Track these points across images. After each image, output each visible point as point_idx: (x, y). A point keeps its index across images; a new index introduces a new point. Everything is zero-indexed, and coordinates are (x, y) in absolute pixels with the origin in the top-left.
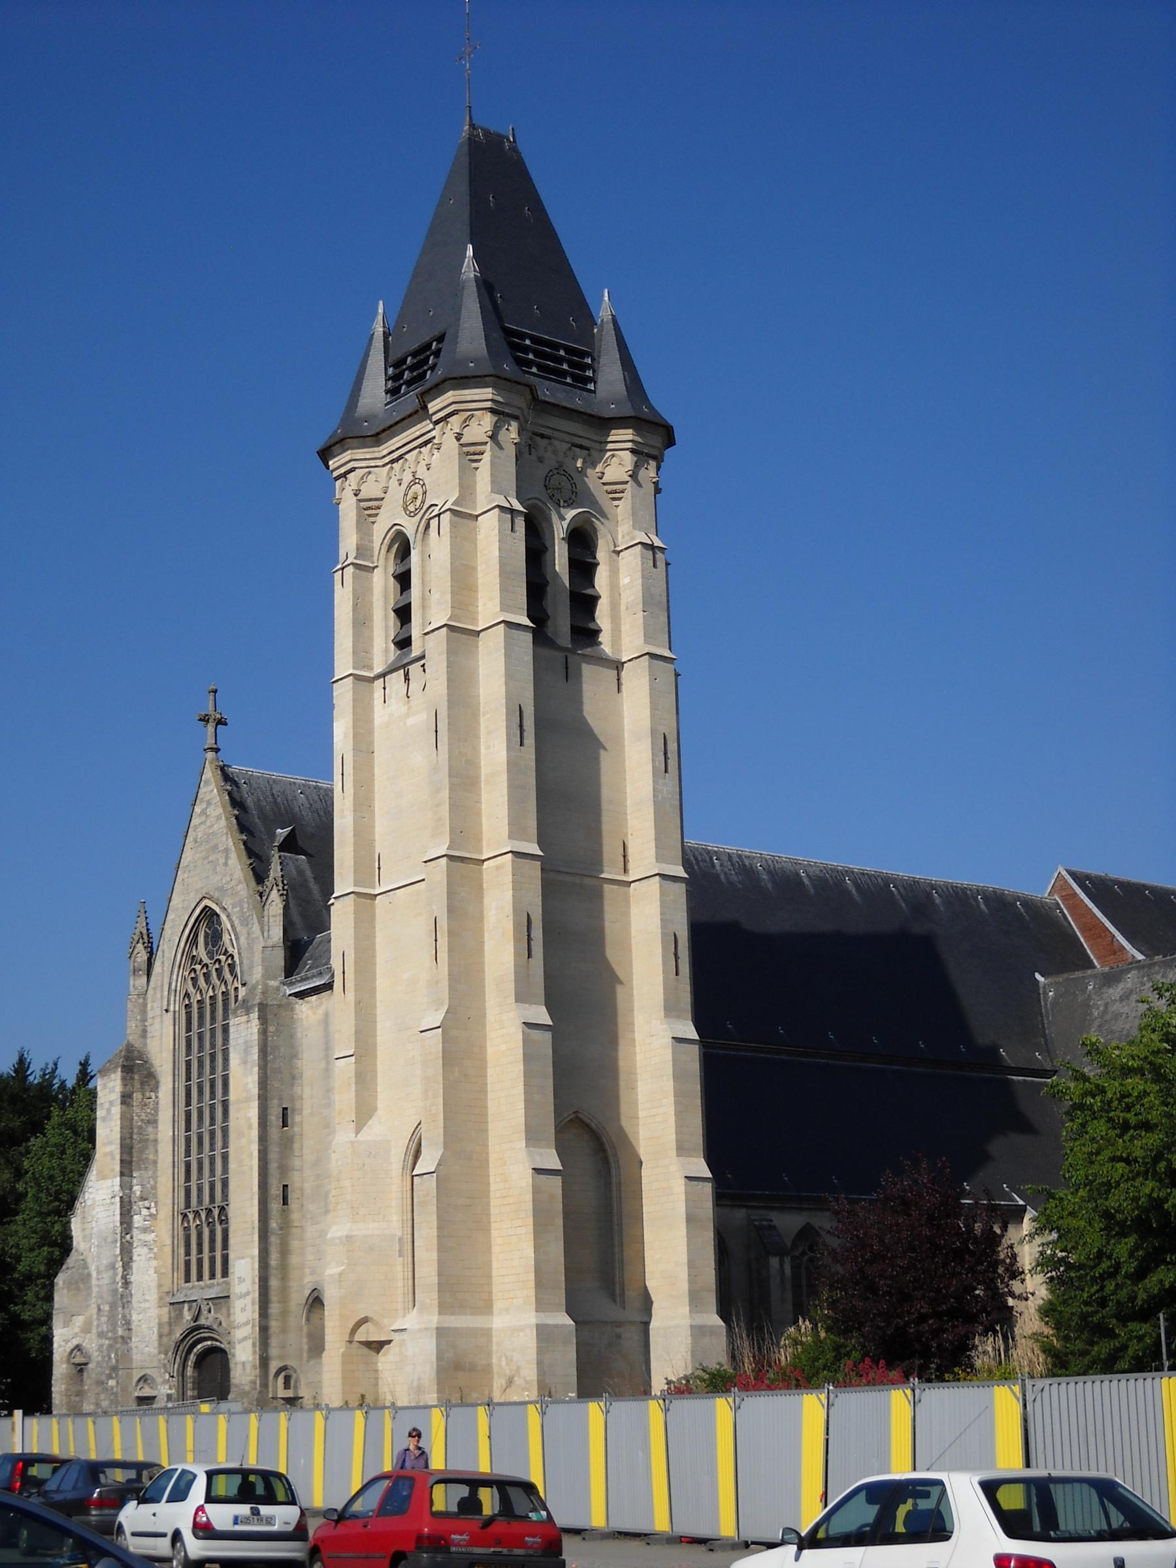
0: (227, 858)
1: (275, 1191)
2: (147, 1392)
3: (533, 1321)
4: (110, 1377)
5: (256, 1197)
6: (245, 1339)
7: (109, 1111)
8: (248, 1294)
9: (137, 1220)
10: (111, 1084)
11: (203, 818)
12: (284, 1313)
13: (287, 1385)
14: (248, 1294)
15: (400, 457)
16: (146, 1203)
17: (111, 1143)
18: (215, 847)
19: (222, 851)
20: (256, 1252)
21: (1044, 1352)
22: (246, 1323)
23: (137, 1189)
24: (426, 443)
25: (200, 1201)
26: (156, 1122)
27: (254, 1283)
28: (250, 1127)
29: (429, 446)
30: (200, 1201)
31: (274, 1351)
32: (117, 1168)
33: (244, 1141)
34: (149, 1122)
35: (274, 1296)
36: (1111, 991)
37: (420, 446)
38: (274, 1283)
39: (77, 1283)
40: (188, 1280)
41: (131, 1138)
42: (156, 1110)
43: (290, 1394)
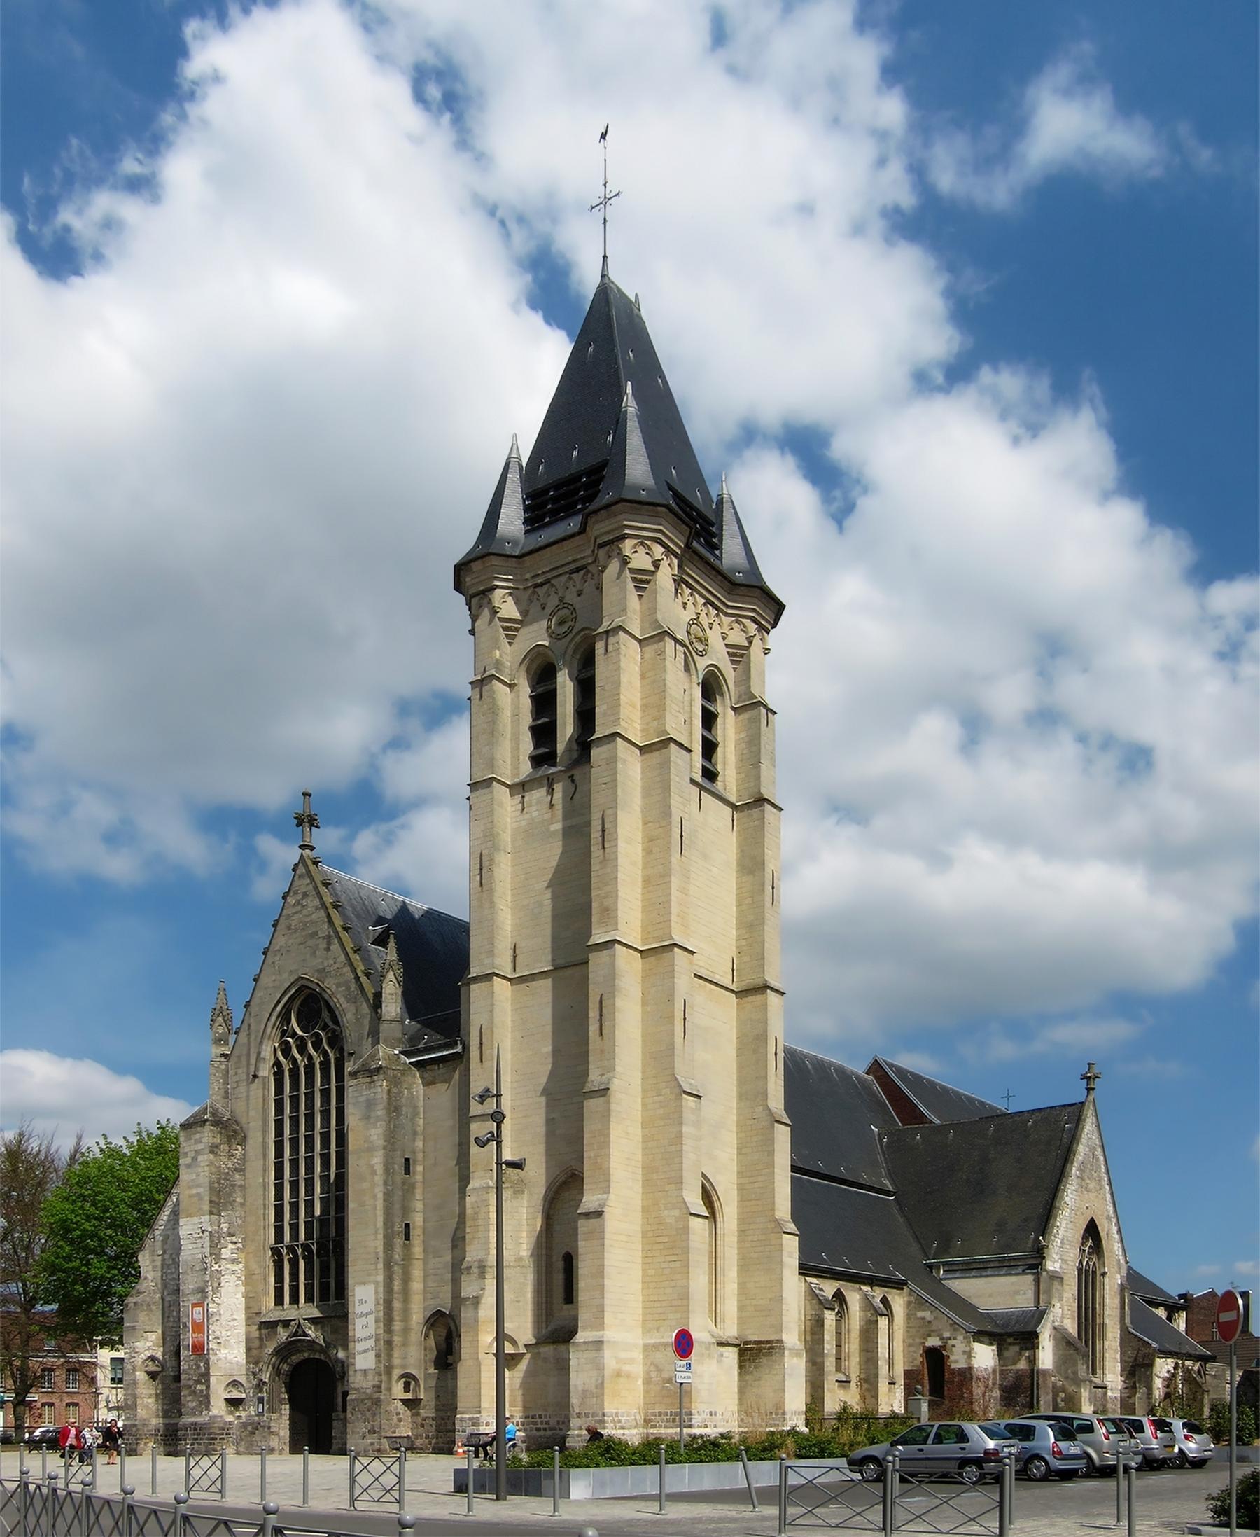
0: (329, 944)
1: (398, 1228)
2: (236, 1394)
3: (641, 1342)
4: (199, 1382)
5: (381, 1231)
6: (366, 1351)
7: (194, 1159)
8: (370, 1313)
9: (226, 1253)
10: (198, 1136)
11: (299, 908)
12: (406, 1330)
13: (407, 1388)
14: (370, 1313)
15: (547, 582)
16: (234, 1239)
17: (198, 1186)
18: (316, 933)
19: (324, 938)
20: (380, 1278)
21: (657, 1439)
22: (370, 1337)
23: (225, 1227)
24: (578, 570)
25: (295, 1236)
26: (243, 1170)
27: (377, 1304)
28: (374, 1173)
29: (582, 573)
30: (295, 1236)
31: (396, 1361)
32: (206, 1207)
33: (365, 1185)
34: (236, 1170)
35: (397, 1316)
36: (380, 1131)
37: (572, 572)
38: (397, 1305)
39: (149, 1305)
40: (279, 1300)
41: (219, 1183)
42: (244, 1159)
43: (409, 1396)
